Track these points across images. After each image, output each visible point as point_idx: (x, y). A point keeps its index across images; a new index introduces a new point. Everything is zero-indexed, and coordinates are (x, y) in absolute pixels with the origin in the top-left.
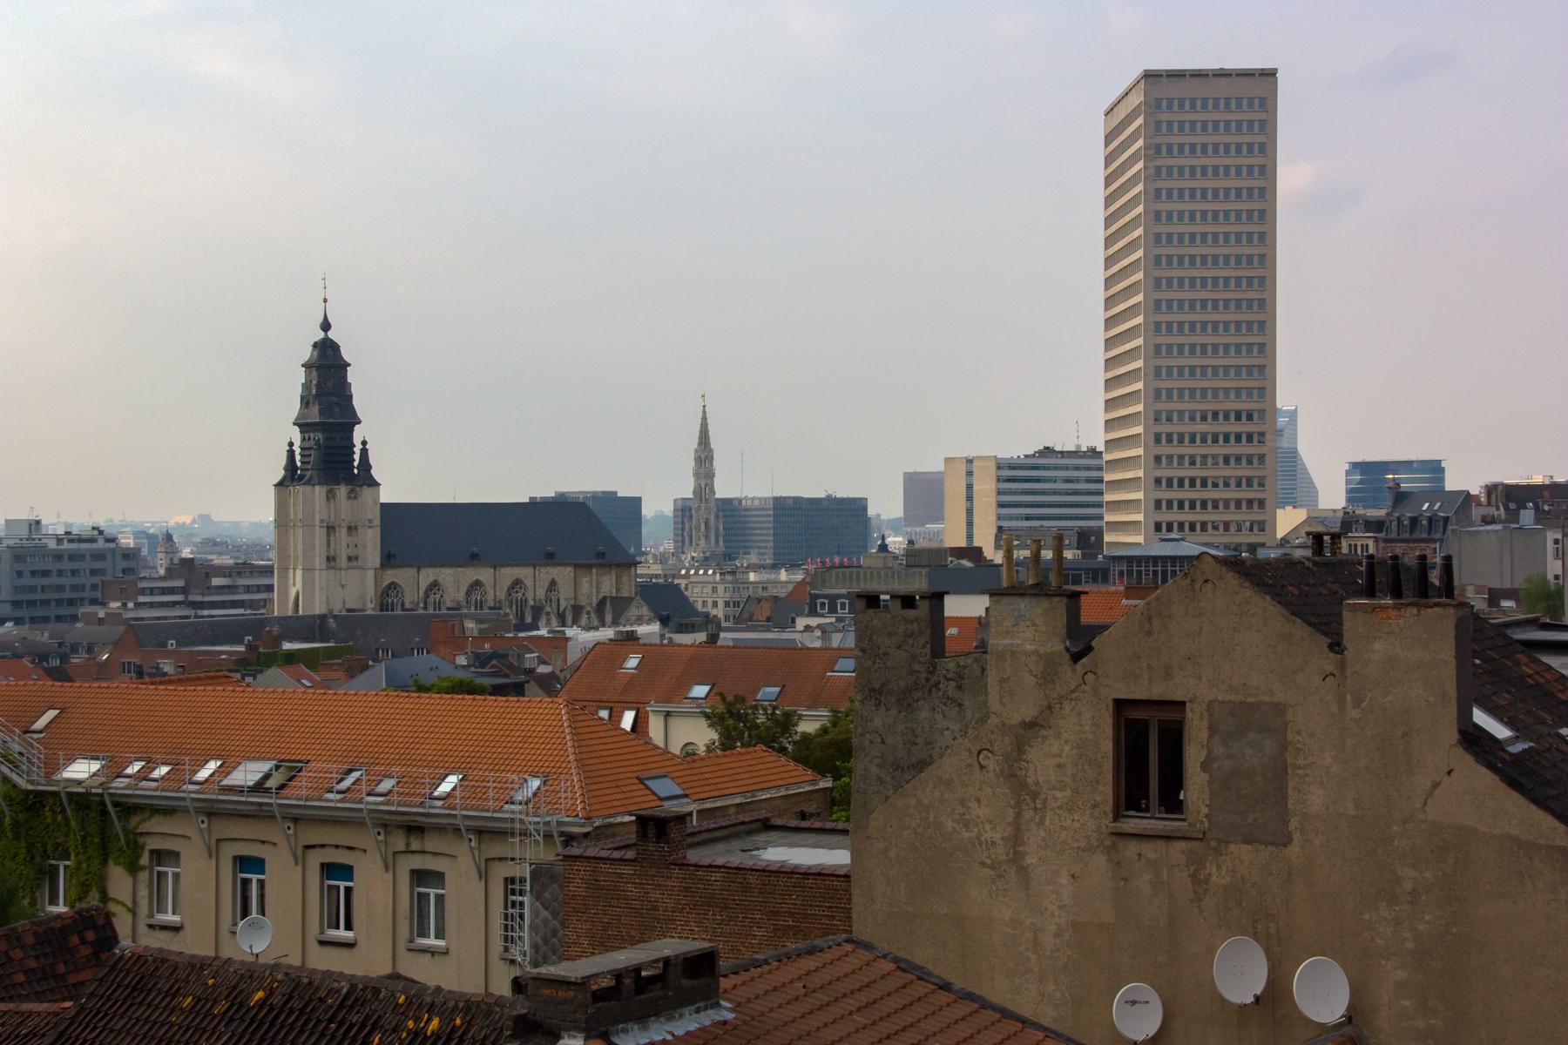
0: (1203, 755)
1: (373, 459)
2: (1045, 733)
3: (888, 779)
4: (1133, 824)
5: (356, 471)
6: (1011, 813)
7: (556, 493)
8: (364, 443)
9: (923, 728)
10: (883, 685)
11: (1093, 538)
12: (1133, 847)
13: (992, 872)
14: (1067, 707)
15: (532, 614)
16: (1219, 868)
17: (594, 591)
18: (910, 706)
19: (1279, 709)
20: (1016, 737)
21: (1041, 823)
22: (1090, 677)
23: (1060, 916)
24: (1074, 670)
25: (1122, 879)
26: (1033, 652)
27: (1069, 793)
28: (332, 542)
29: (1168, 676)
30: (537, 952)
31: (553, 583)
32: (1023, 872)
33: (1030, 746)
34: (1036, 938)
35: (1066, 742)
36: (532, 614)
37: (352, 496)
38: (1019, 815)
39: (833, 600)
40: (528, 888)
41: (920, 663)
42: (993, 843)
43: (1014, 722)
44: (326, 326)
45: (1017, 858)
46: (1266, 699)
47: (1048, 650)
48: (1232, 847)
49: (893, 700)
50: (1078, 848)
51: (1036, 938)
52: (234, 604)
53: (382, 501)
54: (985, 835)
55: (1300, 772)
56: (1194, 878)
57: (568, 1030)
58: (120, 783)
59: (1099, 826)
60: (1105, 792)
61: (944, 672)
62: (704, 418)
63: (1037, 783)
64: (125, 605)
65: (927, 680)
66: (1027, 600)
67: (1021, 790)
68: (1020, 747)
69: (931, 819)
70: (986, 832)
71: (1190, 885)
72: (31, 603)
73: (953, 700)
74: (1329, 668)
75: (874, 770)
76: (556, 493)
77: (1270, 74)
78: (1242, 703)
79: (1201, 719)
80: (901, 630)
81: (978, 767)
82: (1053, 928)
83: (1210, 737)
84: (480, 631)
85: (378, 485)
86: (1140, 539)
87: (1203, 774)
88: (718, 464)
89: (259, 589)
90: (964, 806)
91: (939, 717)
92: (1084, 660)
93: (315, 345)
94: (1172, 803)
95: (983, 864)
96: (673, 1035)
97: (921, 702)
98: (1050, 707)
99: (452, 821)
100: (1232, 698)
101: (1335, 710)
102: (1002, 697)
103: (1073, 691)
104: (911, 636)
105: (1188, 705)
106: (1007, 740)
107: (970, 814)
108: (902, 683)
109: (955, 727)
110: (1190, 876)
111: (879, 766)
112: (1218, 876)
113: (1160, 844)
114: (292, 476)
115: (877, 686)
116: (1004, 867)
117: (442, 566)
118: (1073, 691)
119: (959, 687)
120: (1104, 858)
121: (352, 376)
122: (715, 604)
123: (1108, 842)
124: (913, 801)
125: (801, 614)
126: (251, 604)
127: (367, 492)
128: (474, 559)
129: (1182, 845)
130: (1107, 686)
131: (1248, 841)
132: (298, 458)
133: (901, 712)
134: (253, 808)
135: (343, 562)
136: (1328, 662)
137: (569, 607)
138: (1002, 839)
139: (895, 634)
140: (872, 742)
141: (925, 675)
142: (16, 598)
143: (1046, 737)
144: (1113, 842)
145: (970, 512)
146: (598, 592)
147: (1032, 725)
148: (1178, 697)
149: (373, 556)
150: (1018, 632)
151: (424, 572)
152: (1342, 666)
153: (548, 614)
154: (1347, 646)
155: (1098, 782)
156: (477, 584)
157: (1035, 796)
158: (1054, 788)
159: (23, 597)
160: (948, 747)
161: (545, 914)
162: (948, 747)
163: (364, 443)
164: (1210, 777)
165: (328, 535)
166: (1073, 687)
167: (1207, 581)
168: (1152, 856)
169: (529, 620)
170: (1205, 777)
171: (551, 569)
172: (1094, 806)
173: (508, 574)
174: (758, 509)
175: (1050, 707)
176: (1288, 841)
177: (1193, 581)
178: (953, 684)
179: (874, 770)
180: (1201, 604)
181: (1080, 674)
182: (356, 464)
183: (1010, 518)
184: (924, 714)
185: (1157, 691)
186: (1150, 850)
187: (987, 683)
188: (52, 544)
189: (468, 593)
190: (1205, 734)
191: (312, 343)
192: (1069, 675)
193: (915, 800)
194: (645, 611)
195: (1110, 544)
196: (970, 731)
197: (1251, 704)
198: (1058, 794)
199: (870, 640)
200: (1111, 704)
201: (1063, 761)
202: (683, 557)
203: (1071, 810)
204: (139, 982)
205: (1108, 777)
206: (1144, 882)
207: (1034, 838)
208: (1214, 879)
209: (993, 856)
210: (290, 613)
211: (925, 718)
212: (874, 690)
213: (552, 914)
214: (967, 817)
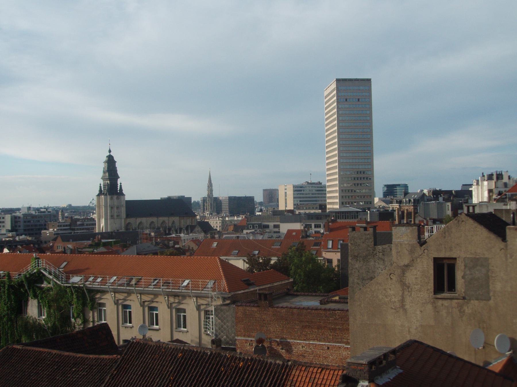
0: (462, 274)
1: (123, 188)
2: (412, 268)
3: (360, 283)
4: (439, 296)
5: (118, 191)
6: (401, 293)
7: (161, 198)
8: (121, 183)
9: (372, 267)
10: (358, 254)
11: (323, 207)
12: (440, 302)
13: (395, 311)
14: (419, 260)
15: (168, 231)
16: (468, 308)
17: (185, 223)
18: (367, 260)
19: (487, 259)
20: (402, 269)
21: (411, 295)
22: (426, 251)
23: (417, 323)
24: (421, 249)
25: (437, 312)
26: (407, 244)
27: (419, 286)
28: (112, 212)
29: (451, 249)
30: (217, 332)
31: (173, 222)
32: (405, 311)
33: (407, 272)
34: (409, 330)
35: (418, 271)
36: (168, 231)
37: (118, 198)
38: (403, 293)
39: (253, 225)
40: (214, 313)
41: (370, 247)
42: (395, 302)
43: (401, 265)
44: (110, 151)
45: (403, 306)
46: (482, 256)
47: (412, 243)
48: (472, 301)
49: (362, 259)
50: (423, 303)
51: (409, 330)
52: (83, 229)
53: (126, 200)
54: (393, 300)
55: (493, 278)
56: (460, 311)
57: (362, 379)
58: (88, 283)
59: (429, 296)
60: (431, 285)
61: (378, 250)
62: (210, 175)
63: (409, 284)
64: (54, 230)
65: (373, 252)
66: (405, 227)
67: (405, 286)
68: (403, 272)
69: (375, 295)
70: (393, 299)
71: (458, 313)
72: (28, 230)
73: (381, 259)
74: (502, 247)
75: (356, 280)
76: (161, 198)
77: (369, 80)
78: (475, 258)
79: (462, 262)
80: (364, 237)
81: (390, 279)
82: (415, 327)
83: (465, 268)
84: (155, 235)
85: (125, 195)
86: (337, 207)
87: (462, 280)
88: (214, 188)
89: (90, 225)
90: (385, 291)
91: (377, 264)
92: (424, 246)
93: (107, 157)
94: (452, 287)
95: (392, 308)
96: (391, 379)
97: (371, 259)
98: (413, 260)
99: (188, 294)
100: (471, 256)
101: (504, 259)
102: (397, 257)
103: (421, 255)
104: (367, 239)
105: (457, 259)
106: (399, 271)
107: (387, 293)
108: (364, 254)
109: (382, 267)
110: (459, 310)
111: (357, 279)
112: (468, 310)
113: (449, 301)
114: (101, 193)
115: (356, 255)
116: (399, 309)
117: (143, 217)
118: (421, 255)
119: (383, 255)
120: (431, 306)
121: (117, 165)
122: (217, 227)
123: (432, 301)
124: (369, 290)
125: (245, 229)
126: (88, 229)
127: (122, 197)
128: (151, 215)
129: (456, 301)
130: (432, 253)
131: (477, 299)
132: (102, 188)
133: (364, 262)
134: (127, 290)
135: (116, 217)
136: (502, 245)
137: (178, 229)
138: (398, 300)
139: (362, 239)
140: (355, 272)
141: (372, 251)
142: (25, 228)
143: (412, 269)
144: (434, 301)
145: (286, 200)
146: (186, 224)
147: (407, 266)
148: (454, 256)
149: (124, 215)
150: (402, 238)
151: (137, 219)
152: (506, 246)
153: (173, 230)
154: (508, 240)
155: (429, 283)
156: (152, 222)
157: (408, 287)
158: (415, 285)
159: (27, 228)
160: (380, 273)
161: (219, 321)
162: (380, 273)
163: (121, 183)
164: (465, 280)
165: (111, 210)
166: (420, 254)
167: (463, 221)
168: (447, 305)
169: (167, 232)
170: (463, 280)
171: (173, 218)
172: (428, 290)
173: (161, 219)
174: (224, 200)
175: (413, 260)
176: (489, 299)
177: (459, 221)
178: (381, 254)
179: (356, 280)
180: (461, 228)
181: (422, 250)
182: (118, 189)
183: (303, 201)
184: (372, 263)
185: (448, 255)
186: (446, 303)
187: (392, 253)
188: (34, 213)
189: (150, 225)
190: (463, 267)
191: (106, 156)
192: (419, 250)
193: (369, 289)
194: (199, 229)
195: (329, 208)
196: (387, 268)
197: (478, 258)
198: (416, 287)
199: (354, 241)
200: (433, 259)
201: (417, 276)
202: (205, 213)
203: (420, 291)
204: (140, 350)
205: (432, 281)
206: (444, 313)
207: (408, 300)
208: (466, 311)
209: (395, 306)
210: (101, 231)
211: (372, 264)
212: (355, 256)
213: (221, 321)
214: (386, 294)
